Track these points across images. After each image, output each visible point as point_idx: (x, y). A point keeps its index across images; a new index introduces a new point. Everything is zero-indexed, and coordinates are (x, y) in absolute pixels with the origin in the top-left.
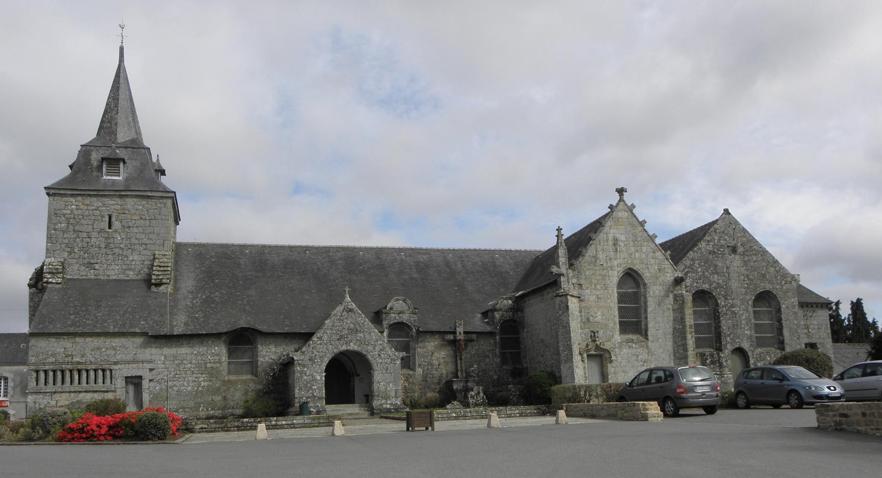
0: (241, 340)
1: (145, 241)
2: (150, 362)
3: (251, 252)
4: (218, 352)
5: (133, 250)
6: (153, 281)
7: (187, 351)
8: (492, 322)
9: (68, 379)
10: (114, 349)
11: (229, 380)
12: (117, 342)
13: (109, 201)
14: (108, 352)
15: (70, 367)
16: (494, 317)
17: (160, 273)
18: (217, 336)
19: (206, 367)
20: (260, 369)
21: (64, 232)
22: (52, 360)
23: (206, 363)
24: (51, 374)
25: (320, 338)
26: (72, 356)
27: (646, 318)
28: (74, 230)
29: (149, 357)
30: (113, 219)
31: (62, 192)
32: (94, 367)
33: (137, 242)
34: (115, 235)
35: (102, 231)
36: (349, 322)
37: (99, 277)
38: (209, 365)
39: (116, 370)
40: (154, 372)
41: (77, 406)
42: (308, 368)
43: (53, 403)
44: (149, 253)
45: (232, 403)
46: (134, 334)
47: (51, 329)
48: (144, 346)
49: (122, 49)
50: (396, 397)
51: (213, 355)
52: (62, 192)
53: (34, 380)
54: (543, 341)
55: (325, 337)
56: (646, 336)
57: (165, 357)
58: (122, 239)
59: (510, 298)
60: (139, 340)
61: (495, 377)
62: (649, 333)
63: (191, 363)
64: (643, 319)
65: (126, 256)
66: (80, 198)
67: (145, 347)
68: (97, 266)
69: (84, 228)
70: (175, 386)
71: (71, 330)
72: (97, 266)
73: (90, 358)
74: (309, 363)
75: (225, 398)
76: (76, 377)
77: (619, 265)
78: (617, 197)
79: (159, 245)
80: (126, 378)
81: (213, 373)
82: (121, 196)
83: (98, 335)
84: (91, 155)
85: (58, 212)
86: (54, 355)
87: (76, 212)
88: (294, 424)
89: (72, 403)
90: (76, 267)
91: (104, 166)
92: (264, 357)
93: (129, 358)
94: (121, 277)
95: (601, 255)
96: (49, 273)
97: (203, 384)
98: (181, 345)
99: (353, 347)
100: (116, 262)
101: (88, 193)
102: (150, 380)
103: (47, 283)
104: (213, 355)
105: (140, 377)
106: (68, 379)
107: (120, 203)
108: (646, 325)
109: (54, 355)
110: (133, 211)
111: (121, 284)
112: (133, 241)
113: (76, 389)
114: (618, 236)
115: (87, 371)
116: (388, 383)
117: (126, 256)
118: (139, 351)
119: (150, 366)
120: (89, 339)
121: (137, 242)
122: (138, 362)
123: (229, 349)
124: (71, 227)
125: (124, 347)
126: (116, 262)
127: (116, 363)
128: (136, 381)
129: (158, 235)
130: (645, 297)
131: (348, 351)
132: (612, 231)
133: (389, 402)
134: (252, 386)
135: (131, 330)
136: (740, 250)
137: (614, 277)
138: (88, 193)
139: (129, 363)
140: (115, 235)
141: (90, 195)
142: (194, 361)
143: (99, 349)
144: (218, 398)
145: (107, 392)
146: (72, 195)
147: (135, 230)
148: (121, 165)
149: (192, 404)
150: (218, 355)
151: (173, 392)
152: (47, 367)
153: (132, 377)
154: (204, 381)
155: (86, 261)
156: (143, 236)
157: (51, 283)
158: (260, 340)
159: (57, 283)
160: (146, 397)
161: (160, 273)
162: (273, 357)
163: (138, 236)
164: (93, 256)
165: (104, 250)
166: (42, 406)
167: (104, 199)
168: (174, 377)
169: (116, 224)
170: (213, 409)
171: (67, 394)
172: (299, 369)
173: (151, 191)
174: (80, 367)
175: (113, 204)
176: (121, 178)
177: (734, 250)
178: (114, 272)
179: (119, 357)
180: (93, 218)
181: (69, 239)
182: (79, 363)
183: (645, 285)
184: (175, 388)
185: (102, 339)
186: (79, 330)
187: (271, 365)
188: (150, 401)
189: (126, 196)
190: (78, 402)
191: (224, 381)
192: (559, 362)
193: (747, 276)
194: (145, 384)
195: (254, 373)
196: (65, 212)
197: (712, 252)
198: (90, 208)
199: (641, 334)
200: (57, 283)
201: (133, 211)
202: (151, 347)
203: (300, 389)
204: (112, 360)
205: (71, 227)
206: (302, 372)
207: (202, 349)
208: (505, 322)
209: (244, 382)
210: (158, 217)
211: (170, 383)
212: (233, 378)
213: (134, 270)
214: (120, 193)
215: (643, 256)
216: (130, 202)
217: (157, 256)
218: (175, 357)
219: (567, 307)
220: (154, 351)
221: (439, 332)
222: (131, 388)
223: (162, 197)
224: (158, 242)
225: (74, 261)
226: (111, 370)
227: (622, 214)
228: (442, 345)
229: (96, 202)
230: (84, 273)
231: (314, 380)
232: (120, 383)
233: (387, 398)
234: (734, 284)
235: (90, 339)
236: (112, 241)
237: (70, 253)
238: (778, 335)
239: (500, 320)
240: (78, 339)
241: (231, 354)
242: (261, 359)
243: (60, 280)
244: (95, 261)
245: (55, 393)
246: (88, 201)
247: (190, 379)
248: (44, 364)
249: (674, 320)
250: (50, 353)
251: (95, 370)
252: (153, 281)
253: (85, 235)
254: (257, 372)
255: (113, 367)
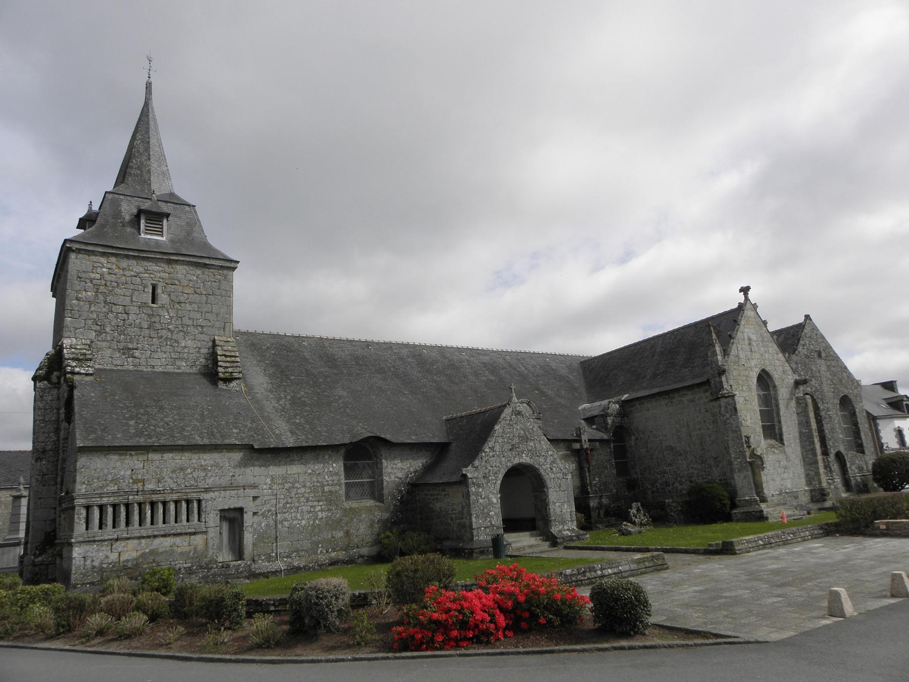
0: (362, 454)
1: (201, 322)
2: (254, 486)
3: (309, 344)
4: (332, 470)
5: (186, 334)
6: (221, 375)
7: (300, 470)
8: (604, 428)
9: (136, 517)
10: (204, 469)
11: (351, 509)
12: (207, 459)
13: (152, 267)
14: (195, 474)
15: (139, 498)
16: (605, 422)
17: (228, 365)
18: (333, 448)
19: (323, 492)
20: (385, 492)
21: (90, 303)
22: (113, 488)
23: (323, 486)
24: (172, 507)
25: (492, 449)
26: (143, 481)
27: (780, 422)
28: (105, 302)
29: (251, 480)
30: (159, 291)
31: (90, 248)
32: (175, 497)
33: (190, 322)
34: (161, 312)
35: (143, 305)
36: (518, 430)
37: (140, 368)
38: (326, 489)
39: (207, 501)
40: (258, 501)
41: (152, 558)
42: (483, 488)
43: (114, 557)
44: (207, 338)
45: (356, 540)
46: (231, 448)
47: (108, 441)
48: (244, 464)
49: (149, 86)
50: (572, 521)
51: (331, 474)
52: (90, 248)
53: (83, 521)
54: (672, 448)
55: (497, 448)
56: (781, 440)
57: (272, 479)
58: (171, 318)
59: (617, 402)
60: (237, 456)
61: (615, 491)
62: (785, 437)
63: (304, 486)
64: (777, 424)
65: (177, 341)
66: (113, 259)
67: (246, 466)
68: (137, 353)
69: (120, 300)
70: (286, 520)
71: (142, 441)
72: (137, 353)
73: (169, 483)
74: (484, 481)
75: (347, 533)
76: (136, 512)
77: (756, 366)
78: (741, 298)
79: (219, 329)
80: (221, 511)
81: (330, 500)
82: (170, 262)
83: (182, 449)
84: (119, 205)
85: (83, 275)
86: (115, 481)
87: (108, 277)
88: (621, 572)
89: (143, 555)
90: (108, 352)
91: (143, 222)
92: (389, 474)
93: (224, 481)
94: (170, 369)
95: (742, 355)
96: (73, 359)
97: (320, 515)
98: (292, 462)
99: (525, 459)
100: (163, 349)
101: (126, 253)
102: (255, 514)
103: (73, 373)
104: (331, 474)
105: (241, 510)
106: (136, 517)
107: (168, 270)
108: (781, 429)
109: (115, 481)
110: (185, 283)
111: (171, 380)
112: (186, 321)
113: (150, 533)
114: (751, 335)
115: (165, 503)
116: (563, 503)
117: (177, 341)
118: (238, 471)
119: (253, 492)
120: (168, 456)
121: (190, 322)
122: (237, 487)
123: (345, 465)
124: (101, 297)
125: (217, 465)
126: (163, 349)
127: (207, 490)
128: (231, 515)
129: (217, 315)
130: (777, 400)
131: (520, 464)
132: (746, 330)
133: (566, 528)
134: (378, 515)
135: (227, 441)
136: (823, 355)
137: (754, 375)
138: (126, 253)
139: (225, 489)
140: (161, 312)
141: (128, 257)
142: (308, 484)
143: (182, 469)
144: (340, 534)
145: (195, 534)
146: (103, 254)
147: (188, 307)
148: (165, 221)
149: (307, 544)
150: (336, 474)
151: (283, 529)
152: (105, 500)
153: (229, 509)
154: (322, 510)
155: (121, 346)
156: (198, 315)
157: (79, 373)
158: (384, 452)
159: (87, 375)
160: (249, 538)
161: (228, 365)
162: (400, 475)
163: (192, 315)
164: (131, 339)
165: (147, 332)
166: (96, 564)
167: (146, 263)
168: (284, 507)
169: (163, 298)
170: (334, 550)
171: (136, 541)
172: (473, 489)
173: (209, 258)
174: (155, 498)
175: (158, 271)
176: (164, 239)
177: (820, 356)
178: (161, 362)
179: (210, 481)
180: (132, 287)
181: (98, 313)
182: (154, 492)
183: (775, 387)
184: (286, 524)
185: (187, 455)
186: (153, 441)
187: (398, 486)
188: (254, 544)
189: (176, 261)
190: (152, 552)
191: (345, 510)
192: (732, 471)
193: (832, 381)
194: (248, 519)
195: (380, 498)
196: (93, 276)
197: (807, 357)
198: (127, 273)
199: (775, 438)
200: (87, 375)
201: (185, 283)
202: (253, 465)
203: (477, 517)
204: (201, 485)
205: (101, 297)
206: (477, 494)
207: (318, 467)
208: (616, 427)
209: (369, 510)
210: (218, 292)
211: (279, 516)
212: (354, 504)
213: (187, 360)
214: (168, 258)
215: (771, 357)
216: (181, 270)
217: (217, 342)
218: (285, 479)
219: (735, 409)
220: (257, 470)
221: (564, 441)
222: (225, 526)
223: (221, 267)
224: (217, 324)
225: (104, 344)
226: (199, 501)
227: (749, 313)
228: (567, 455)
229: (136, 267)
230: (119, 362)
231: (491, 503)
232: (212, 519)
233: (563, 522)
234: (826, 388)
235: (171, 455)
236: (157, 319)
237: (99, 333)
238: (856, 438)
239: (612, 425)
240: (152, 456)
241: (348, 471)
242: (386, 478)
243: (91, 371)
244: (134, 345)
245: (117, 540)
246: (124, 263)
247: (305, 508)
248: (101, 496)
249: (799, 424)
250: (110, 477)
251: (176, 502)
252: (221, 375)
253: (121, 309)
254: (382, 495)
255: (203, 496)
